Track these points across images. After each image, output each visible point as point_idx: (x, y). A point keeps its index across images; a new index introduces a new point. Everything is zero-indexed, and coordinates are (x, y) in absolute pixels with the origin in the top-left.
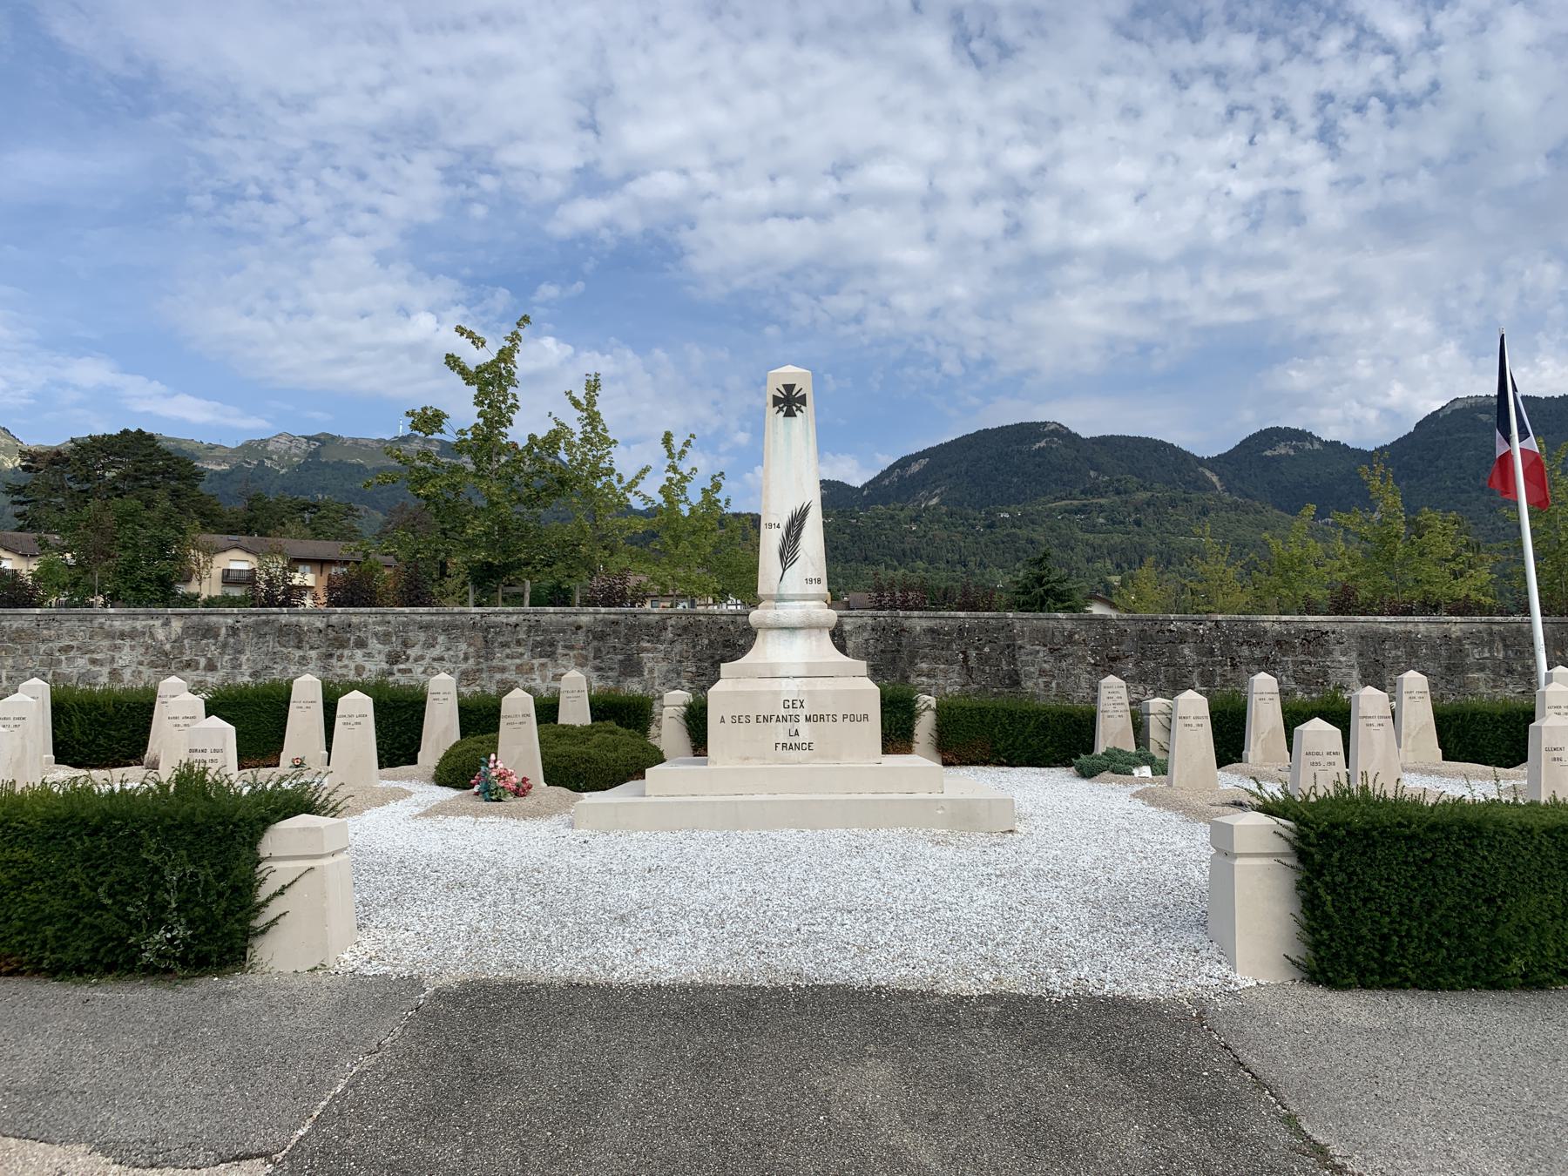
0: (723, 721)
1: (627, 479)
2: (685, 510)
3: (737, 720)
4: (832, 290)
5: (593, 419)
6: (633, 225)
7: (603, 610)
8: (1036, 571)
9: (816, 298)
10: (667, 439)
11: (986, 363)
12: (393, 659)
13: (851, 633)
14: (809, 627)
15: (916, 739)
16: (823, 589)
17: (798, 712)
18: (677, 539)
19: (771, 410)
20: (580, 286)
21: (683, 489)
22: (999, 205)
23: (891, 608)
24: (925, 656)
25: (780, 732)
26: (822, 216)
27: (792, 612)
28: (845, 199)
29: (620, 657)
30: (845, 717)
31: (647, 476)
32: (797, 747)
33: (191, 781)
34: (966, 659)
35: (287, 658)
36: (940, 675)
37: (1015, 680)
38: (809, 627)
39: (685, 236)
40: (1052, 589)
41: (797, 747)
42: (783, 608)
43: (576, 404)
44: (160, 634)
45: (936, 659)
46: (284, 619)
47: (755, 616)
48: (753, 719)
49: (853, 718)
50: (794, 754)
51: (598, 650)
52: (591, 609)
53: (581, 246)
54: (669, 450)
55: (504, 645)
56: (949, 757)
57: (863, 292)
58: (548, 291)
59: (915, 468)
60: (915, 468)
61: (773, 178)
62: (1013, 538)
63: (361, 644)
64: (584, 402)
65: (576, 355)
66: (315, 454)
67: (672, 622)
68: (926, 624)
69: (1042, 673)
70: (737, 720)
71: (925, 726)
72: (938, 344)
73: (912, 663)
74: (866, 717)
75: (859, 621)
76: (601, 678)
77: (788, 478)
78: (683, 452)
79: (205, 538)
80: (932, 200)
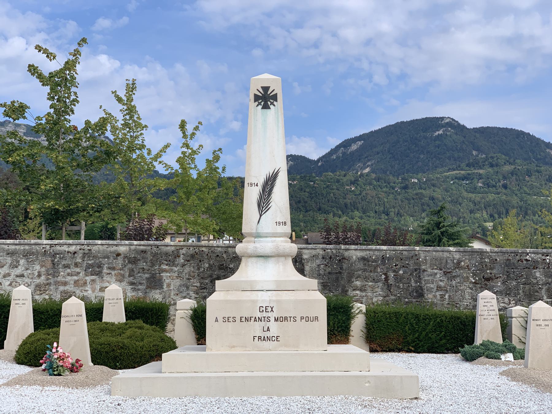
0: (217, 320)
1: (154, 153)
2: (194, 174)
3: (227, 320)
4: (299, 25)
5: (131, 110)
7: (135, 243)
8: (436, 219)
9: (288, 31)
10: (183, 126)
11: (403, 77)
13: (308, 260)
14: (278, 255)
15: (352, 333)
16: (288, 229)
17: (269, 314)
18: (188, 194)
19: (253, 104)
20: (125, 20)
21: (193, 160)
25: (257, 329)
27: (266, 245)
29: (147, 276)
30: (302, 318)
31: (168, 150)
32: (269, 339)
34: (387, 279)
36: (369, 289)
37: (420, 293)
38: (278, 255)
40: (446, 231)
41: (269, 339)
43: (119, 100)
45: (366, 279)
47: (240, 248)
48: (238, 319)
49: (308, 319)
51: (131, 271)
52: (127, 242)
55: (67, 266)
56: (374, 346)
57: (320, 27)
58: (104, 23)
59: (354, 147)
60: (354, 147)
64: (125, 98)
65: (122, 67)
67: (183, 251)
68: (360, 254)
69: (439, 288)
70: (227, 320)
71: (358, 325)
72: (371, 63)
73: (350, 281)
74: (316, 318)
75: (314, 252)
76: (134, 290)
77: (265, 151)
78: (193, 134)
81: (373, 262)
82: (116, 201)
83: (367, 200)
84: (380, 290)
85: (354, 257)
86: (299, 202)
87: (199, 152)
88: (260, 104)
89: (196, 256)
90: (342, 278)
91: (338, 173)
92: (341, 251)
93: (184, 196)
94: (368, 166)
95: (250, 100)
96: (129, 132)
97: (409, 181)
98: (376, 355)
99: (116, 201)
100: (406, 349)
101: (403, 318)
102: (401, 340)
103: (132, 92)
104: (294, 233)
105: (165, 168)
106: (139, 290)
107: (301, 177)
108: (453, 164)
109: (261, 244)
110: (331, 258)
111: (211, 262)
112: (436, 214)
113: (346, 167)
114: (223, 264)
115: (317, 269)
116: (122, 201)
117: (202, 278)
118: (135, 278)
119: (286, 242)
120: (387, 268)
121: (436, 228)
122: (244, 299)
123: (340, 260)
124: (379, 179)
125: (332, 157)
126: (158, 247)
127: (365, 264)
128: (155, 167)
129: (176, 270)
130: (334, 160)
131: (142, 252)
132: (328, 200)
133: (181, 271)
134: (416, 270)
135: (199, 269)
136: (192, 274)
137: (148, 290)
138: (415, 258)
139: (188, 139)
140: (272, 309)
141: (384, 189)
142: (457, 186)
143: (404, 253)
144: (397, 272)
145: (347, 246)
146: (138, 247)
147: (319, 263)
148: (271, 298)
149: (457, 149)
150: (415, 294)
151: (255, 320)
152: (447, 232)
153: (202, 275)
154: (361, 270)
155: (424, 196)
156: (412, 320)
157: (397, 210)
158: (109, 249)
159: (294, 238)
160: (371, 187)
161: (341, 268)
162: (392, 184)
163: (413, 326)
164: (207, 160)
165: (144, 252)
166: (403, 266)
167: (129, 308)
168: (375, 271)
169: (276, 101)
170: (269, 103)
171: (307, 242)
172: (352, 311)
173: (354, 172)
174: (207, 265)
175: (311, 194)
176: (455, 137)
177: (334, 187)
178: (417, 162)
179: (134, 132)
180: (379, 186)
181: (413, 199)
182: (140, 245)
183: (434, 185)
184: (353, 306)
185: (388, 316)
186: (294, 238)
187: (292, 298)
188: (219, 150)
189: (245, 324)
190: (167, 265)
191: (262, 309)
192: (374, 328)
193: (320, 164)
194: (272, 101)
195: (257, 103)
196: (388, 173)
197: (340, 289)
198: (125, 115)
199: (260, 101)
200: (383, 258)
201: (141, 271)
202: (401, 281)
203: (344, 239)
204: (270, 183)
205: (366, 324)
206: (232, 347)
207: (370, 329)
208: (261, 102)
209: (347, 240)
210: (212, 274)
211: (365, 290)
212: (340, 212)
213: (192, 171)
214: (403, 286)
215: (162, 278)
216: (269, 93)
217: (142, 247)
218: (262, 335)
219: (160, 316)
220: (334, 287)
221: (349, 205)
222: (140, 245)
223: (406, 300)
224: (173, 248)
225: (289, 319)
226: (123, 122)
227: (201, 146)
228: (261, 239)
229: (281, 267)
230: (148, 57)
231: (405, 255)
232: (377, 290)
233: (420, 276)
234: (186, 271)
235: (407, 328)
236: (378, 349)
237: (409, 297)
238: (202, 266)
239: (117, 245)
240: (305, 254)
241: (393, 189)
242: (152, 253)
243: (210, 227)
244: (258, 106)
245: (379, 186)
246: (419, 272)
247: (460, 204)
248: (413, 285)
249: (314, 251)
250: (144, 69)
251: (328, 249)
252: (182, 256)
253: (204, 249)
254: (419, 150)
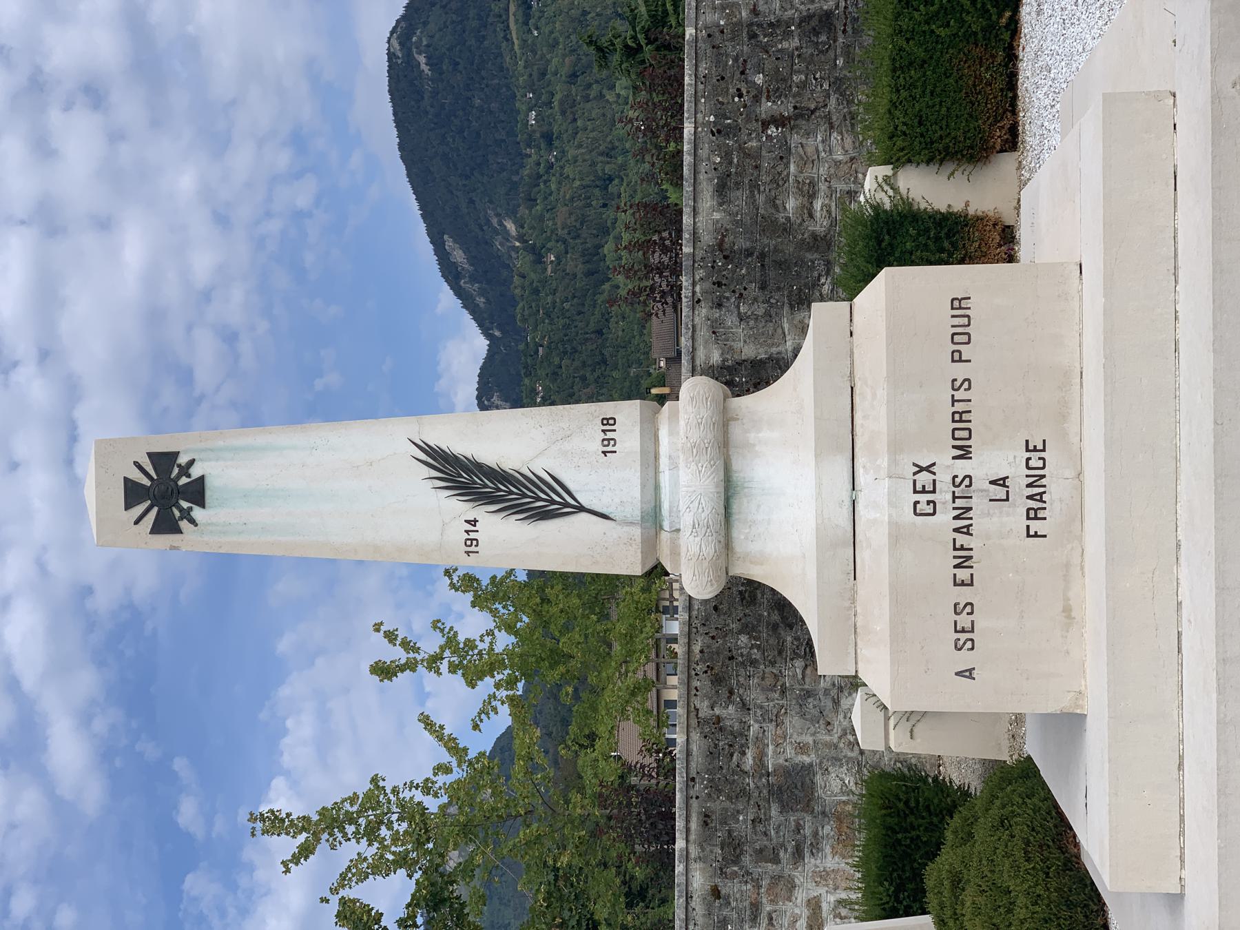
0: (968, 674)
1: (445, 757)
2: (504, 641)
3: (965, 637)
4: (185, 377)
5: (331, 822)
6: (86, 681)
7: (680, 844)
8: (616, 58)
9: (200, 400)
10: (384, 671)
11: (298, 141)
13: (727, 350)
14: (723, 448)
15: (958, 207)
16: (627, 412)
17: (944, 478)
18: (557, 657)
19: (189, 539)
20: (180, 764)
21: (470, 644)
22: (55, 116)
23: (676, 270)
24: (772, 202)
25: (998, 525)
26: (72, 391)
27: (687, 490)
28: (45, 355)
29: (774, 811)
30: (957, 358)
31: (437, 720)
32: (1036, 480)
34: (779, 121)
36: (810, 172)
38: (723, 448)
39: (103, 601)
40: (646, 32)
41: (1036, 480)
42: (674, 510)
43: (305, 851)
45: (779, 181)
47: (695, 581)
48: (964, 595)
49: (961, 336)
50: (1056, 490)
51: (760, 854)
52: (679, 868)
53: (118, 763)
54: (402, 668)
56: (999, 135)
57: (189, 328)
58: (188, 813)
59: (458, 256)
60: (458, 256)
61: (14, 466)
62: (569, 105)
64: (302, 838)
65: (287, 773)
67: (704, 706)
68: (707, 200)
70: (965, 637)
71: (930, 189)
72: (268, 215)
73: (786, 229)
74: (958, 304)
75: (703, 333)
76: (816, 848)
77: (359, 493)
78: (406, 645)
80: (48, 220)
81: (731, 163)
82: (567, 879)
83: (578, 225)
84: (811, 141)
85: (716, 216)
86: (583, 378)
87: (451, 628)
88: (186, 515)
89: (716, 671)
90: (776, 250)
91: (518, 291)
92: (700, 254)
93: (562, 669)
94: (501, 224)
95: (173, 548)
96: (389, 826)
97: (534, 131)
98: (1031, 134)
99: (567, 879)
100: (1006, 36)
101: (911, 47)
102: (977, 52)
103: (283, 820)
104: (654, 391)
105: (492, 714)
106: (815, 834)
107: (528, 375)
108: (495, 31)
109: (682, 507)
110: (719, 284)
111: (734, 626)
112: (605, 57)
113: (505, 273)
114: (741, 592)
115: (752, 323)
116: (564, 860)
117: (780, 653)
118: (782, 845)
119: (674, 416)
120: (748, 120)
121: (640, 57)
122: (885, 570)
123: (726, 257)
124: (531, 200)
125: (482, 305)
126: (693, 779)
127: (737, 184)
128: (482, 754)
129: (757, 726)
130: (488, 301)
131: (706, 823)
132: (579, 313)
133: (759, 712)
134: (753, 36)
135: (754, 663)
136: (769, 681)
137: (818, 809)
138: (718, 39)
139: (419, 658)
140: (921, 469)
141: (553, 187)
142: (543, 21)
143: (703, 70)
144: (759, 90)
145: (686, 236)
146: (692, 837)
147: (735, 319)
148: (884, 473)
149: (462, 21)
150: (823, 38)
151: (966, 531)
152: (649, 30)
153: (771, 654)
154: (754, 196)
155: (567, 96)
156: (916, 14)
157: (601, 158)
158: (700, 920)
159: (666, 390)
160: (547, 216)
161: (749, 253)
162: (542, 170)
163: (938, 12)
164: (474, 605)
165: (706, 819)
166: (743, 73)
167: (885, 899)
168: (755, 155)
169: (175, 455)
170: (184, 481)
171: (675, 360)
172: (888, 206)
173: (514, 255)
174: (744, 639)
175: (565, 353)
176: (432, 27)
177: (549, 299)
178: (491, 112)
179: (389, 811)
180: (546, 198)
181: (575, 120)
182: (688, 830)
183: (543, 74)
184: (871, 206)
185: (904, 94)
186: (666, 390)
187: (882, 393)
188: (450, 576)
189: (979, 568)
190: (744, 753)
191: (923, 507)
192: (941, 137)
193: (497, 333)
194: (176, 470)
195: (184, 524)
196: (515, 178)
197: (809, 256)
198: (345, 835)
199: (177, 513)
200: (718, 132)
201: (760, 828)
202: (784, 80)
203: (665, 250)
205: (929, 162)
206: (1069, 617)
207: (946, 148)
208: (181, 510)
209: (668, 242)
210: (768, 624)
211: (812, 184)
212: (607, 286)
213: (499, 648)
214: (799, 72)
215: (781, 766)
216: (146, 482)
217: (694, 825)
218: (1020, 505)
219: (907, 803)
220: (804, 274)
221: (588, 266)
222: (688, 830)
223: (840, 62)
224: (695, 736)
225: (959, 407)
226: (364, 841)
227: (436, 625)
228: (665, 506)
229: (765, 434)
230: (263, 716)
231: (710, 69)
232: (810, 150)
233: (771, 25)
234: (761, 699)
235: (942, 32)
236: (1006, 123)
237: (831, 54)
238: (745, 652)
239: (689, 898)
240: (708, 357)
241: (551, 166)
242: (709, 795)
243: (637, 602)
244: (193, 521)
245: (546, 198)
246: (760, 25)
247: (585, 13)
248: (796, 42)
249: (698, 329)
250: (289, 723)
251: (694, 293)
252: (717, 711)
253: (697, 648)
254: (464, 109)
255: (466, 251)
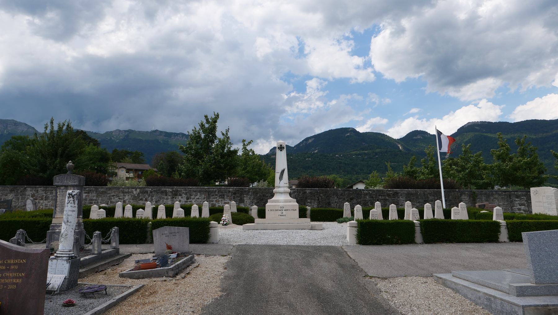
12: (188, 199)
14: (285, 193)
16: (288, 185)
25: (280, 213)
27: (281, 190)
33: (195, 218)
34: (318, 199)
35: (163, 198)
37: (329, 204)
38: (285, 193)
44: (135, 193)
46: (163, 189)
49: (293, 210)
51: (234, 197)
55: (213, 195)
59: (310, 141)
63: (180, 195)
66: (127, 136)
69: (335, 202)
79: (114, 164)
204: (283, 172)
255: (312, 142)
